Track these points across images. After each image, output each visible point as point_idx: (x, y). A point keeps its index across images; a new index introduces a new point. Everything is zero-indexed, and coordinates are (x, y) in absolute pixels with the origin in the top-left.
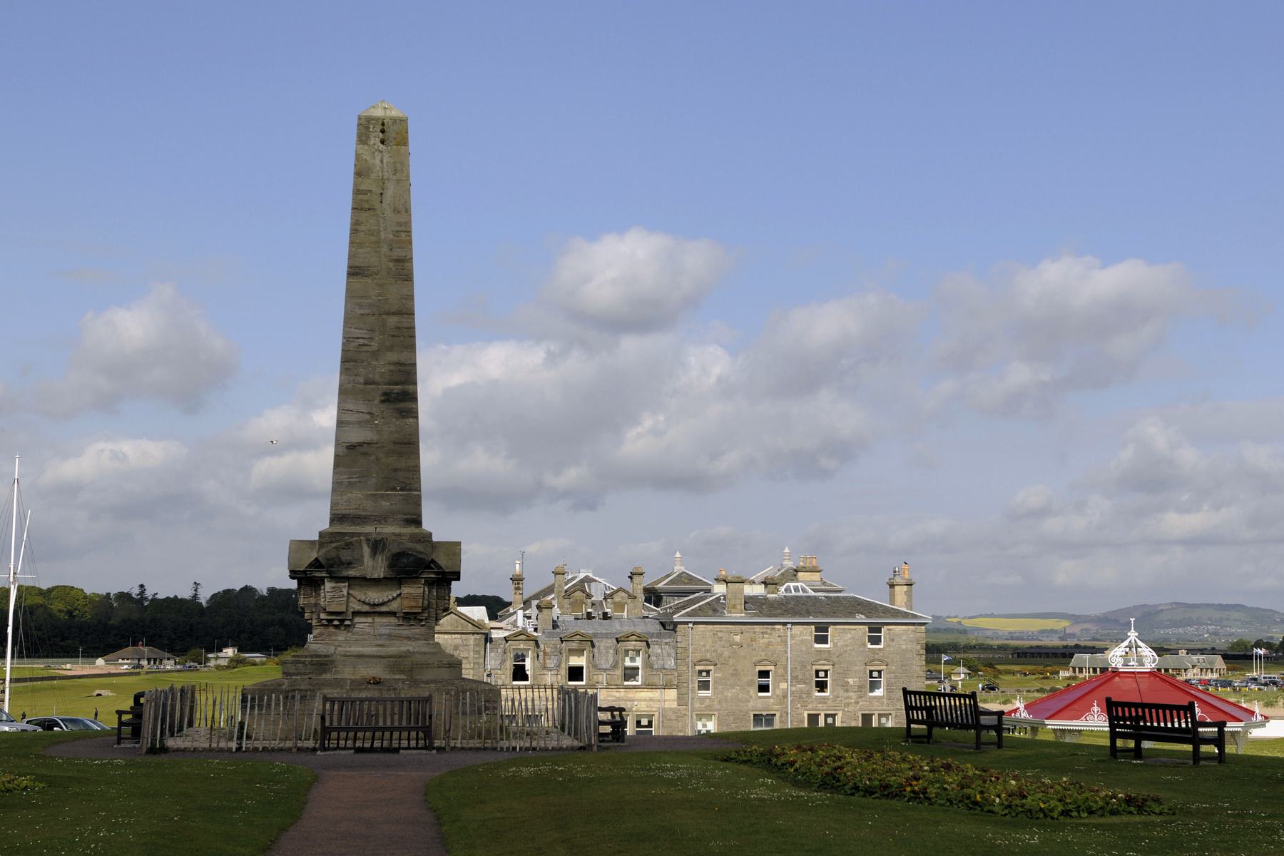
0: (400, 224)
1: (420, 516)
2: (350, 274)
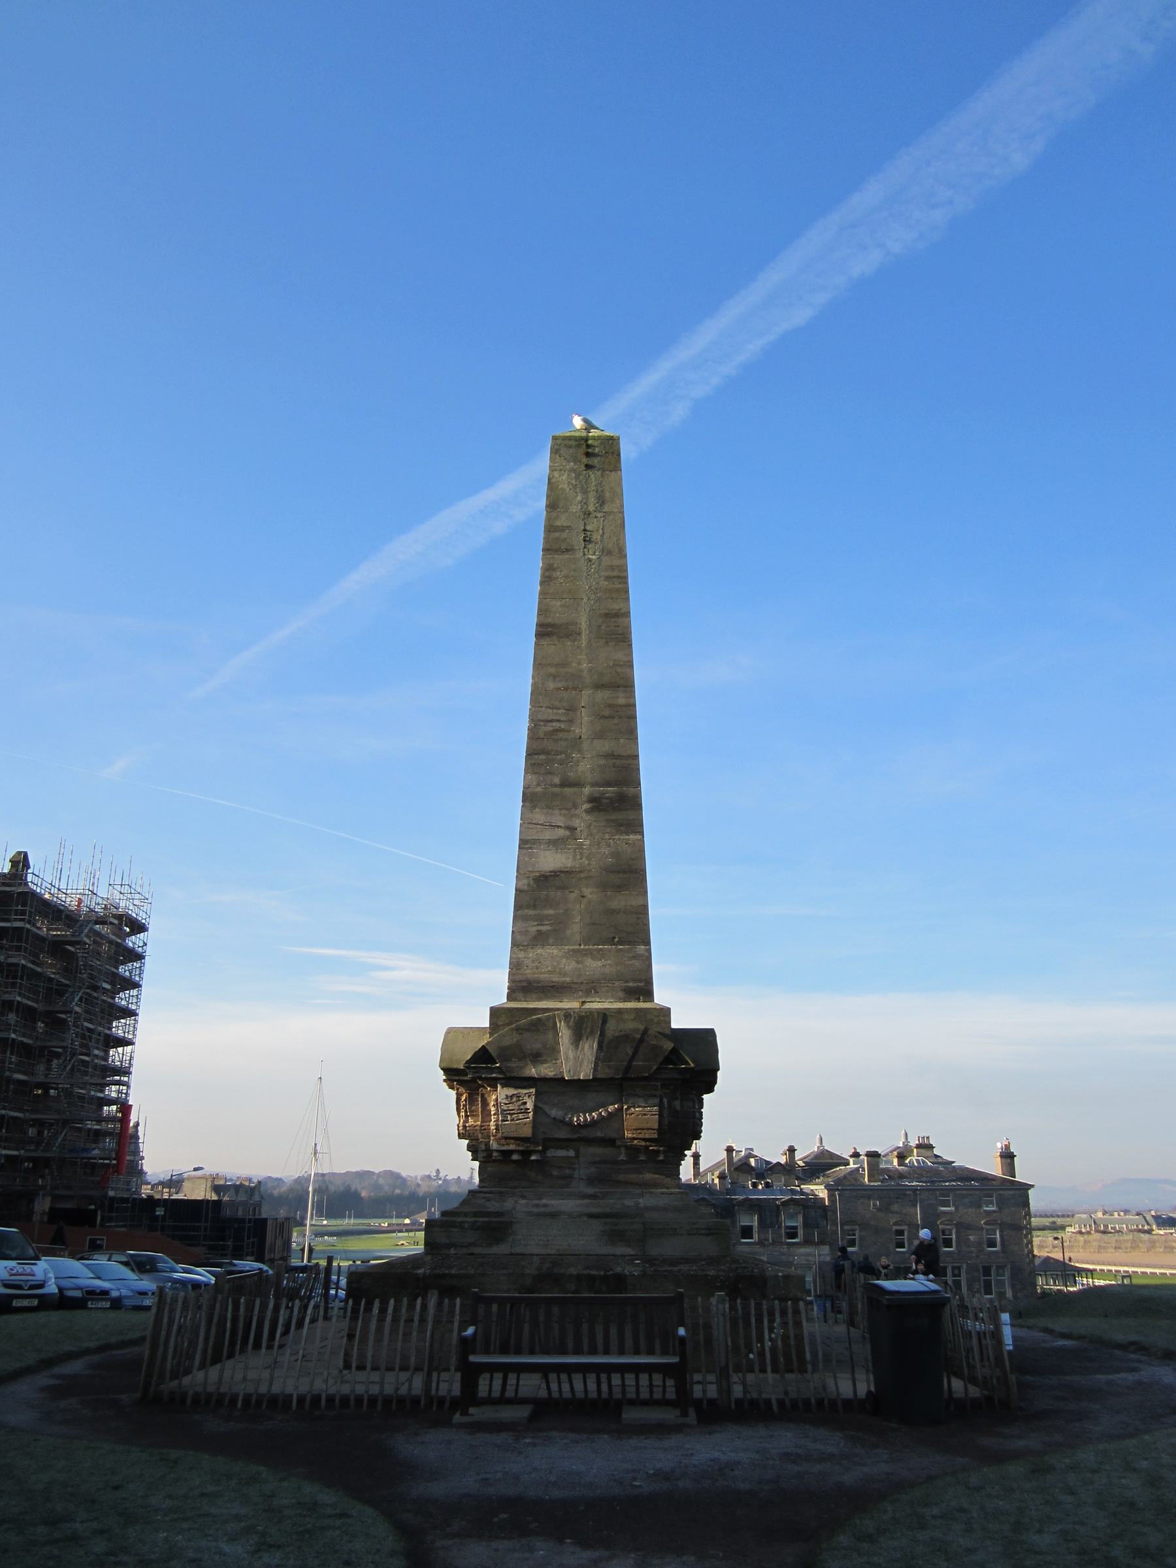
0: (612, 568)
1: (649, 982)
2: (539, 635)
